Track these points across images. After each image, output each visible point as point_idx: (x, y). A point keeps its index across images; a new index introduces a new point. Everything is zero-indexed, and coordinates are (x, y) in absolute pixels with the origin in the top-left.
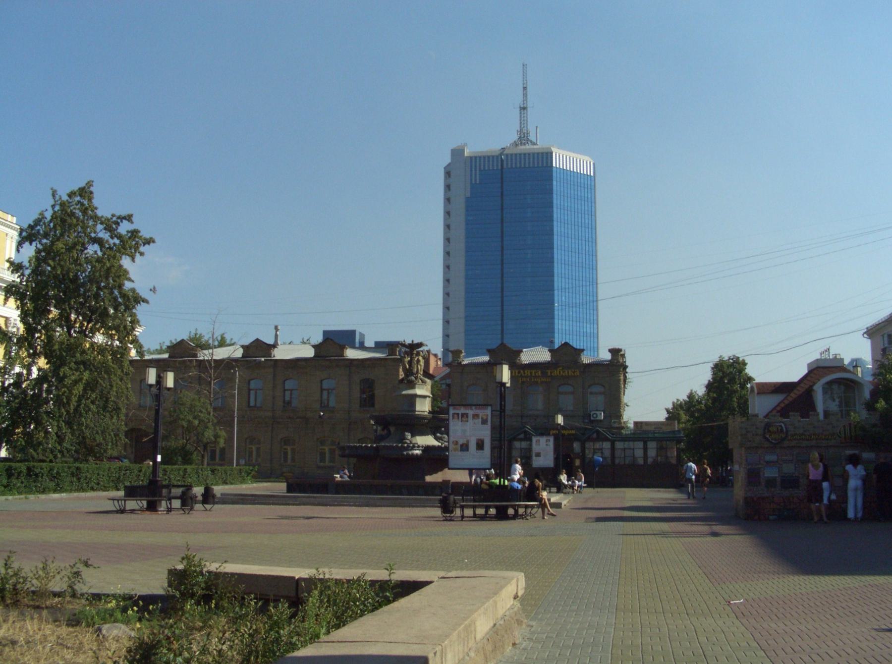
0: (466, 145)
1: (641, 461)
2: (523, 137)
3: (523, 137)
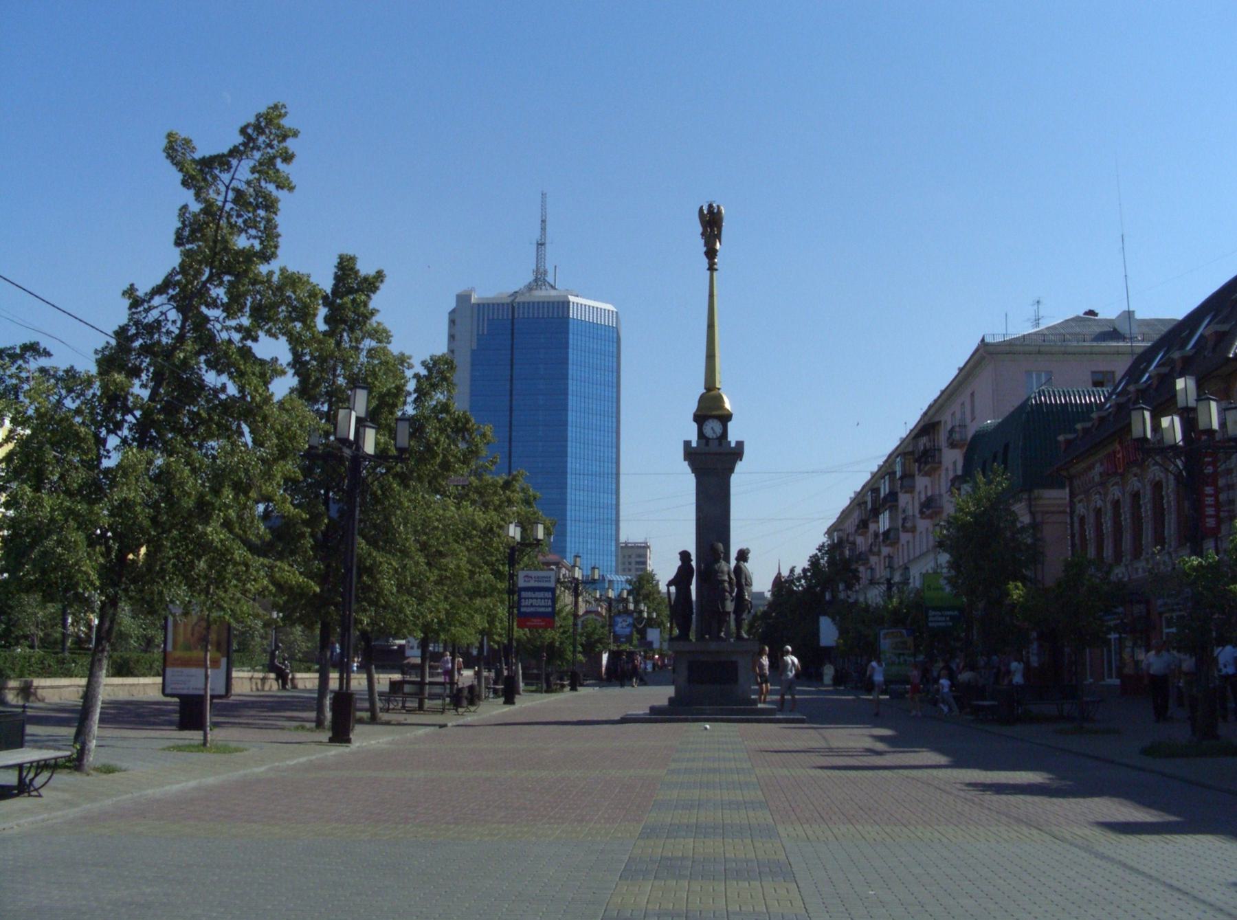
0: (473, 289)
1: (134, 421)
2: (540, 279)
3: (540, 279)
